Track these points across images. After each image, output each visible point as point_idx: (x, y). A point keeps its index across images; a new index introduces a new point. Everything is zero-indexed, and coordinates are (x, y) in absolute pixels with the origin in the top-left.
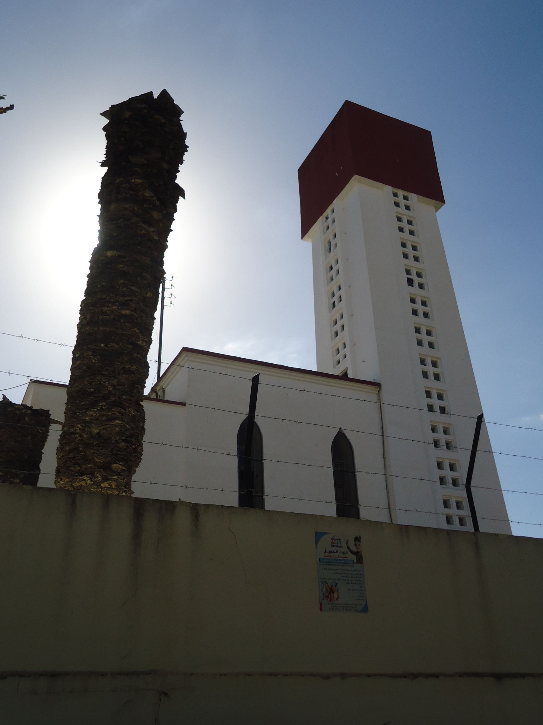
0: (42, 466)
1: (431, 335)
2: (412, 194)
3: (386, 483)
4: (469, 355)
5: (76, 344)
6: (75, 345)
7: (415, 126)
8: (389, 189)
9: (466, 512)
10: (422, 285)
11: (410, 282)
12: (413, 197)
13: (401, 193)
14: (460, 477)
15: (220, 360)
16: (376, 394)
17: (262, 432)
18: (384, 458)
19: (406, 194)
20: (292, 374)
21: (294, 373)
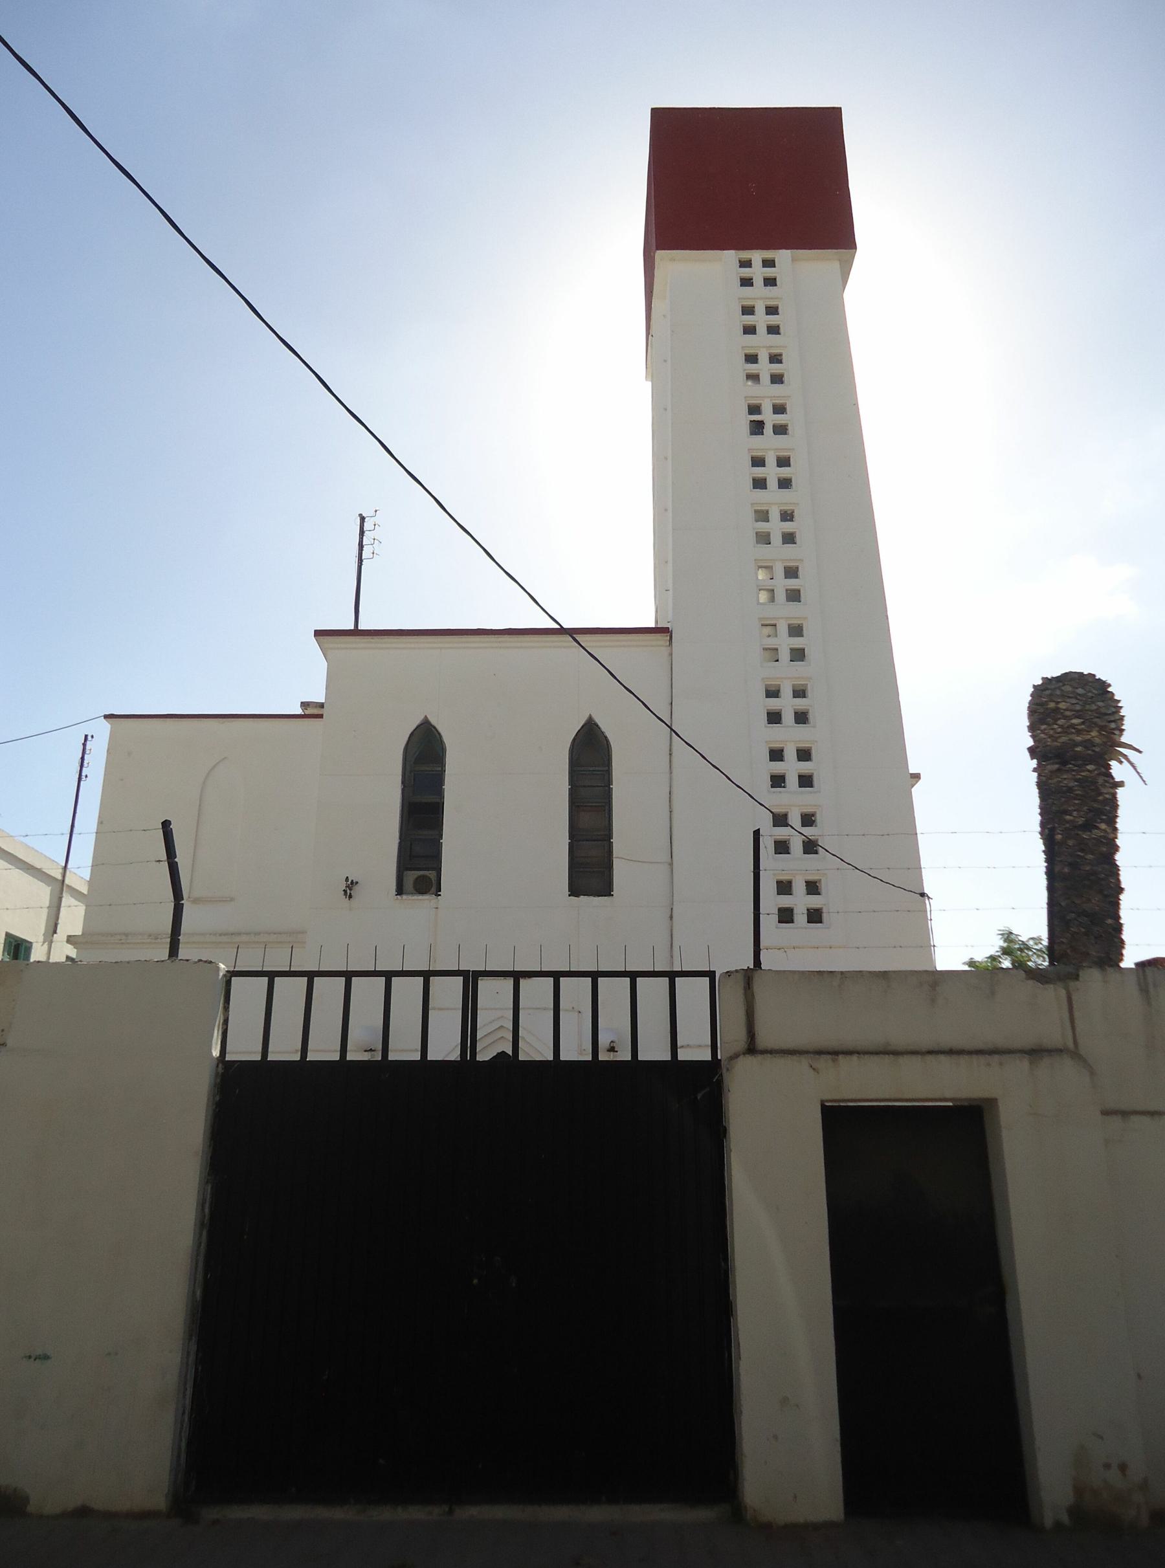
0: (92, 838)
1: (793, 517)
2: (781, 251)
3: (670, 798)
4: (885, 600)
5: (1111, 771)
6: (1111, 769)
7: (803, 108)
8: (730, 257)
9: (771, 901)
10: (785, 426)
11: (757, 428)
12: (783, 256)
13: (757, 256)
14: (815, 770)
15: (376, 639)
16: (667, 646)
17: (445, 741)
18: (670, 754)
19: (769, 254)
20: (500, 639)
21: (506, 638)
